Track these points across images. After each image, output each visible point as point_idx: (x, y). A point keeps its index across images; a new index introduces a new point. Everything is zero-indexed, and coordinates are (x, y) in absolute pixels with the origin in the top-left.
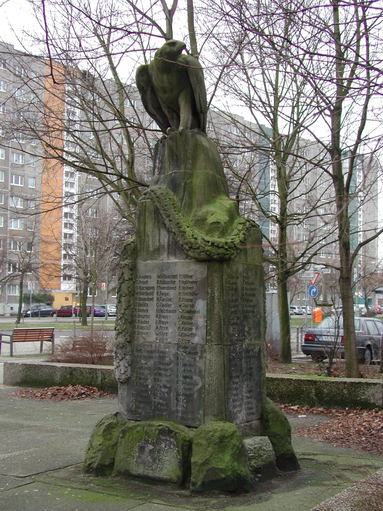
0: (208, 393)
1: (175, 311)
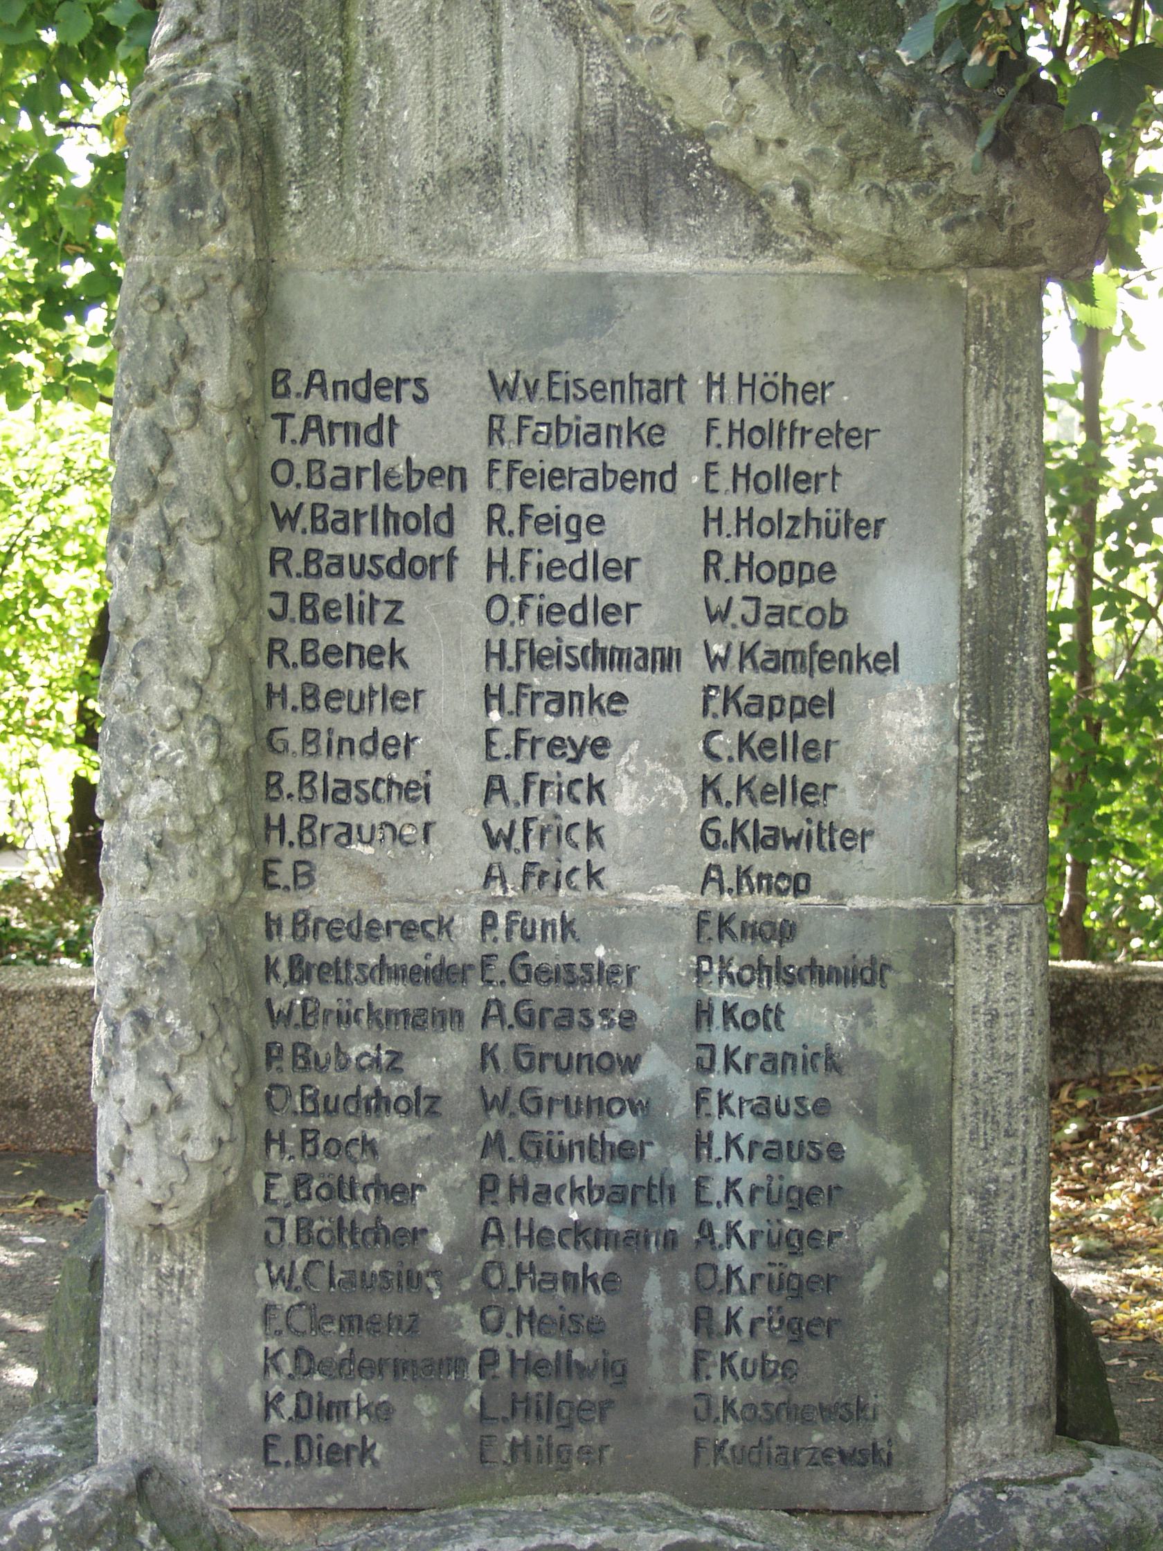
0: (985, 1250)
1: (667, 660)
